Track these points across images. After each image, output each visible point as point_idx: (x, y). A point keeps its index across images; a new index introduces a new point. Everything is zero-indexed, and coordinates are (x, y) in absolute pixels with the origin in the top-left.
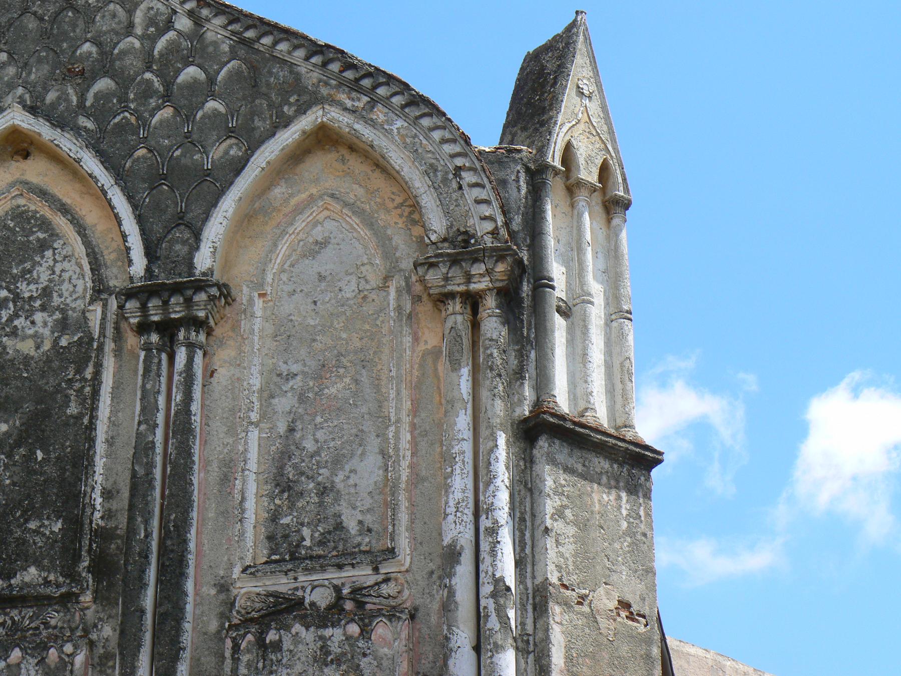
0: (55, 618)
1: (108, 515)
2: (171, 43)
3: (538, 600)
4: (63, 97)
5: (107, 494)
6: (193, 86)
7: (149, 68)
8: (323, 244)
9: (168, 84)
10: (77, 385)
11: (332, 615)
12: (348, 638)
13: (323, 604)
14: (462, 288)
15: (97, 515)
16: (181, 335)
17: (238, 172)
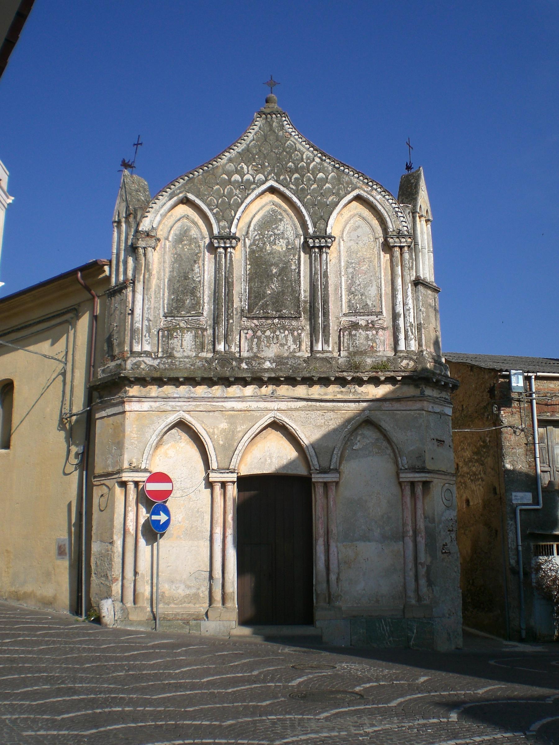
0: (294, 323)
1: (305, 297)
2: (314, 165)
3: (419, 327)
4: (285, 179)
5: (305, 291)
6: (321, 179)
7: (309, 172)
8: (358, 227)
9: (315, 178)
10: (294, 261)
11: (367, 328)
12: (373, 335)
13: (364, 325)
14: (399, 245)
15: (303, 297)
16: (324, 250)
17: (337, 205)
